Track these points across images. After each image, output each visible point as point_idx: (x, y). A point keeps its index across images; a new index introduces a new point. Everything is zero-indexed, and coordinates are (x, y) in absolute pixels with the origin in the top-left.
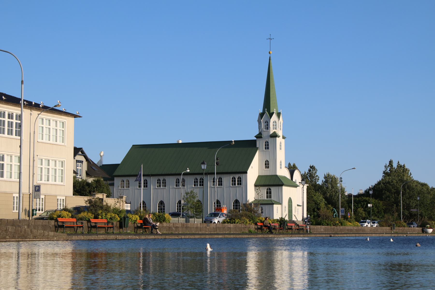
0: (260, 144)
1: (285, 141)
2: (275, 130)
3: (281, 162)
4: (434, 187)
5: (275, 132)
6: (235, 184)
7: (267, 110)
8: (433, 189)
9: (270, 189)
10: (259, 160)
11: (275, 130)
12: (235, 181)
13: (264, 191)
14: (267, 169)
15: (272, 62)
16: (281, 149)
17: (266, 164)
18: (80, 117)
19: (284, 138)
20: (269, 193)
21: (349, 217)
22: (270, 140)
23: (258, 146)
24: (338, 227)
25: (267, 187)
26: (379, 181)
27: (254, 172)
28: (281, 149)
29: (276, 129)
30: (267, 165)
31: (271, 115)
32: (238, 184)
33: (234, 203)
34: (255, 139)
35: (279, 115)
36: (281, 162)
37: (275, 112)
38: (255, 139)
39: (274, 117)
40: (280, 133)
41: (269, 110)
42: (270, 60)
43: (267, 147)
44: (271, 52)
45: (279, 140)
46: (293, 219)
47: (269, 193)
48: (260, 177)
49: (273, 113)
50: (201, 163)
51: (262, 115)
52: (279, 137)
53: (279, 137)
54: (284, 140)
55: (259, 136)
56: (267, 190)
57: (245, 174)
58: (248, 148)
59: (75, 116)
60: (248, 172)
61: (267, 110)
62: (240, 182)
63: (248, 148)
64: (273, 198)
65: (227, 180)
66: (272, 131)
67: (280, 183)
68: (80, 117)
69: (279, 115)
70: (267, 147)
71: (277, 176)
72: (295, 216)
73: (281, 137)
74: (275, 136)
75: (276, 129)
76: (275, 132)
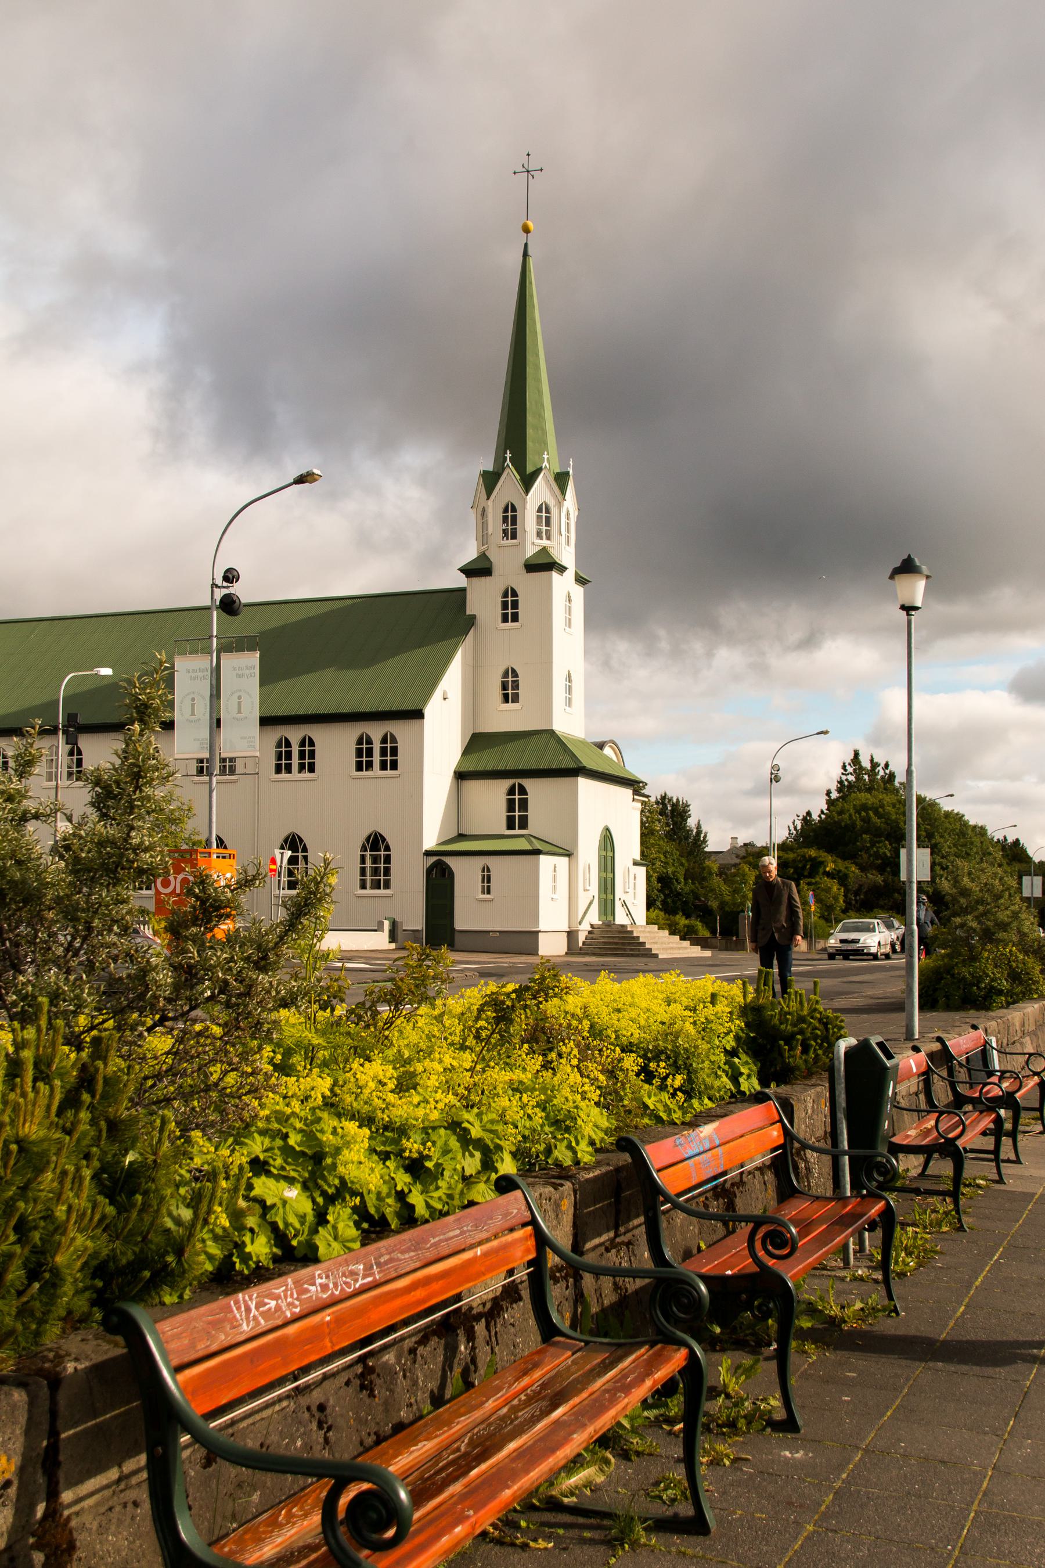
2: (545, 542)
5: (544, 550)
8: (1041, 863)
9: (523, 791)
11: (545, 542)
14: (510, 706)
16: (569, 702)
17: (505, 605)
19: (580, 580)
20: (517, 814)
22: (526, 585)
25: (507, 783)
28: (569, 702)
30: (510, 691)
31: (528, 481)
32: (383, 767)
33: (364, 848)
34: (460, 581)
35: (561, 479)
39: (541, 490)
40: (566, 556)
42: (525, 255)
43: (510, 608)
45: (563, 586)
47: (517, 814)
50: (165, 1309)
51: (490, 480)
52: (562, 569)
53: (562, 569)
56: (511, 791)
60: (428, 711)
62: (382, 757)
63: (426, 623)
64: (535, 826)
66: (531, 546)
67: (567, 763)
69: (561, 479)
71: (552, 733)
72: (624, 904)
73: (570, 574)
74: (543, 565)
76: (544, 550)
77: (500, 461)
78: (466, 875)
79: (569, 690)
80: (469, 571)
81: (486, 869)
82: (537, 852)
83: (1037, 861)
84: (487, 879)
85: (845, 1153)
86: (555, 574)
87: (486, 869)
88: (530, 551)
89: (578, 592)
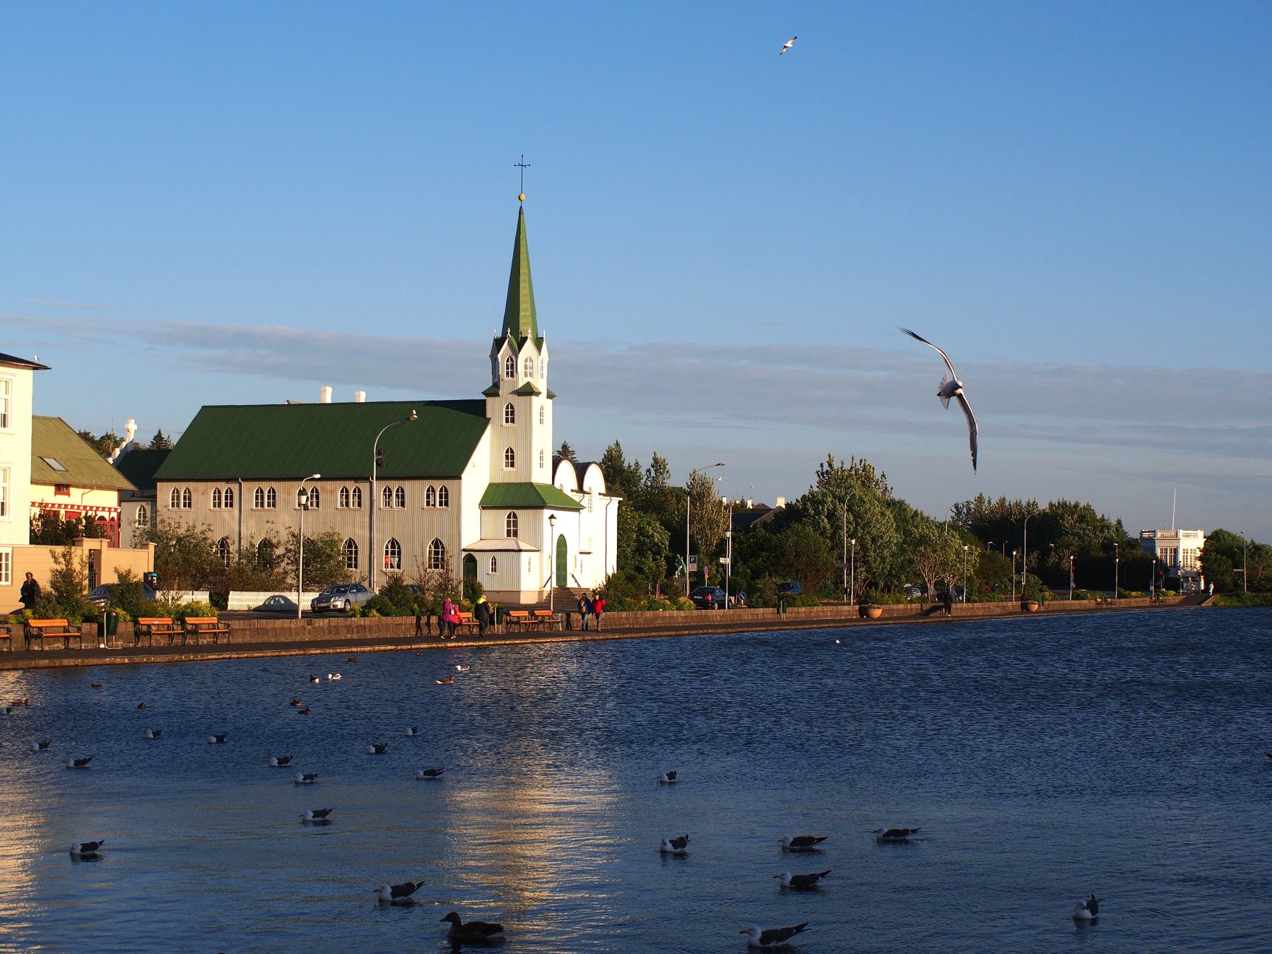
0: (495, 408)
1: (553, 403)
2: (529, 379)
3: (542, 452)
4: (1271, 525)
5: (528, 383)
6: (347, 505)
7: (512, 332)
9: (515, 516)
10: (492, 446)
12: (220, 498)
13: (500, 518)
15: (526, 216)
18: (46, 368)
19: (550, 396)
21: (918, 605)
22: (518, 402)
23: (489, 415)
24: (710, 612)
25: (508, 512)
26: (1071, 500)
27: (481, 470)
29: (531, 375)
30: (510, 458)
32: (441, 504)
34: (483, 397)
35: (538, 343)
36: (542, 452)
37: (529, 336)
38: (483, 397)
39: (529, 346)
40: (541, 384)
41: (516, 332)
43: (511, 416)
44: (523, 197)
45: (540, 403)
46: (569, 585)
48: (492, 487)
49: (526, 338)
51: (498, 343)
52: (538, 394)
54: (550, 401)
55: (493, 391)
56: (509, 517)
57: (456, 481)
58: (466, 419)
59: (37, 367)
60: (465, 475)
61: (512, 332)
65: (416, 490)
66: (522, 381)
67: (538, 503)
68: (46, 368)
70: (511, 416)
71: (531, 484)
73: (544, 394)
74: (528, 391)
75: (531, 375)
76: (528, 383)
77: (505, 332)
78: (484, 563)
79: (541, 458)
80: (487, 393)
81: (494, 558)
82: (520, 551)
83: (943, 514)
84: (494, 563)
85: (219, 600)
86: (534, 398)
87: (494, 558)
88: (521, 384)
89: (549, 403)
